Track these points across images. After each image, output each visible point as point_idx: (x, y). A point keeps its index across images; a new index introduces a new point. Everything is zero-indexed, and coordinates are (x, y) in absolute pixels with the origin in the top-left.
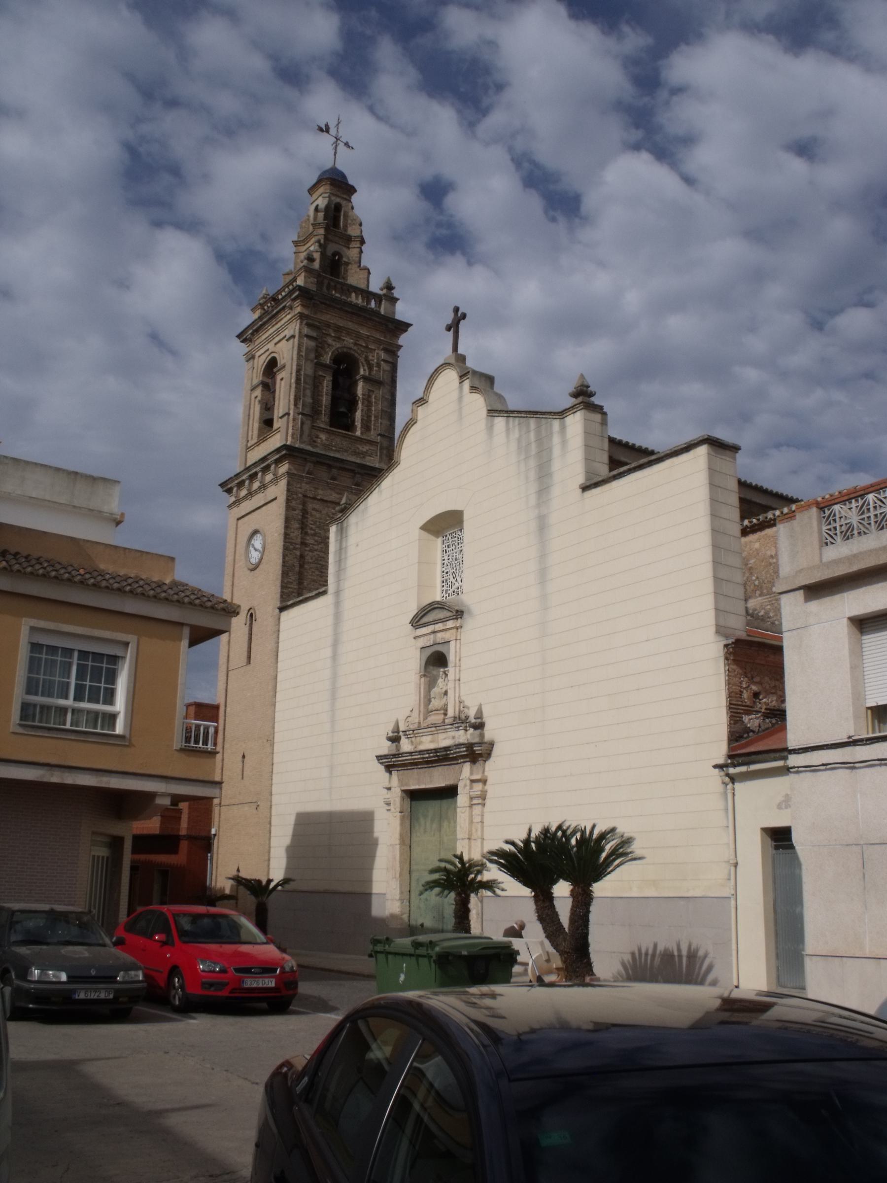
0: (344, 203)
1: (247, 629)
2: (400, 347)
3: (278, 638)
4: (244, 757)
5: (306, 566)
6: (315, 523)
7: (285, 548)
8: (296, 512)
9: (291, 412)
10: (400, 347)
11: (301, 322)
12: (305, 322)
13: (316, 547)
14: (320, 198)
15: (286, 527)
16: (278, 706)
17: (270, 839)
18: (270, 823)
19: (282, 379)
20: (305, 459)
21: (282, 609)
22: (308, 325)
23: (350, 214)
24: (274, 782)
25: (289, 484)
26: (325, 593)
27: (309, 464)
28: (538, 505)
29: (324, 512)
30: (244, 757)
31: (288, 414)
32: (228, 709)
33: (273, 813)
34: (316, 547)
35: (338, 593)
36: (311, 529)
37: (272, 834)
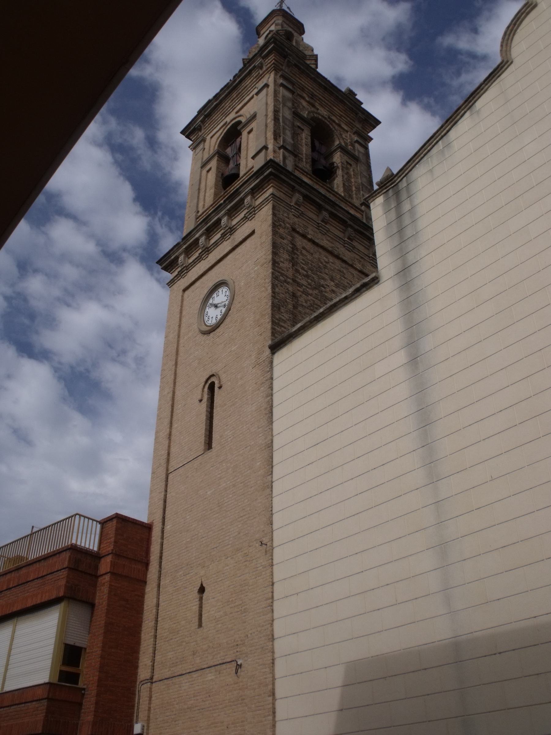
0: (295, 34)
1: (203, 407)
2: (371, 139)
3: (271, 388)
4: (202, 590)
5: (300, 309)
6: (306, 264)
7: (275, 277)
8: (285, 241)
9: (270, 147)
10: (371, 139)
11: (276, 74)
12: (279, 75)
13: (310, 291)
14: (274, 25)
15: (274, 253)
16: (277, 488)
17: (274, 726)
18: (273, 694)
19: (249, 132)
20: (293, 188)
21: (275, 348)
22: (282, 76)
23: (301, 43)
24: (276, 615)
25: (274, 208)
26: (375, 281)
27: (297, 194)
28: (153, 676)
29: (316, 256)
30: (202, 590)
31: (265, 148)
32: (168, 527)
33: (279, 672)
34: (310, 291)
35: (404, 272)
36: (303, 269)
37: (278, 716)
